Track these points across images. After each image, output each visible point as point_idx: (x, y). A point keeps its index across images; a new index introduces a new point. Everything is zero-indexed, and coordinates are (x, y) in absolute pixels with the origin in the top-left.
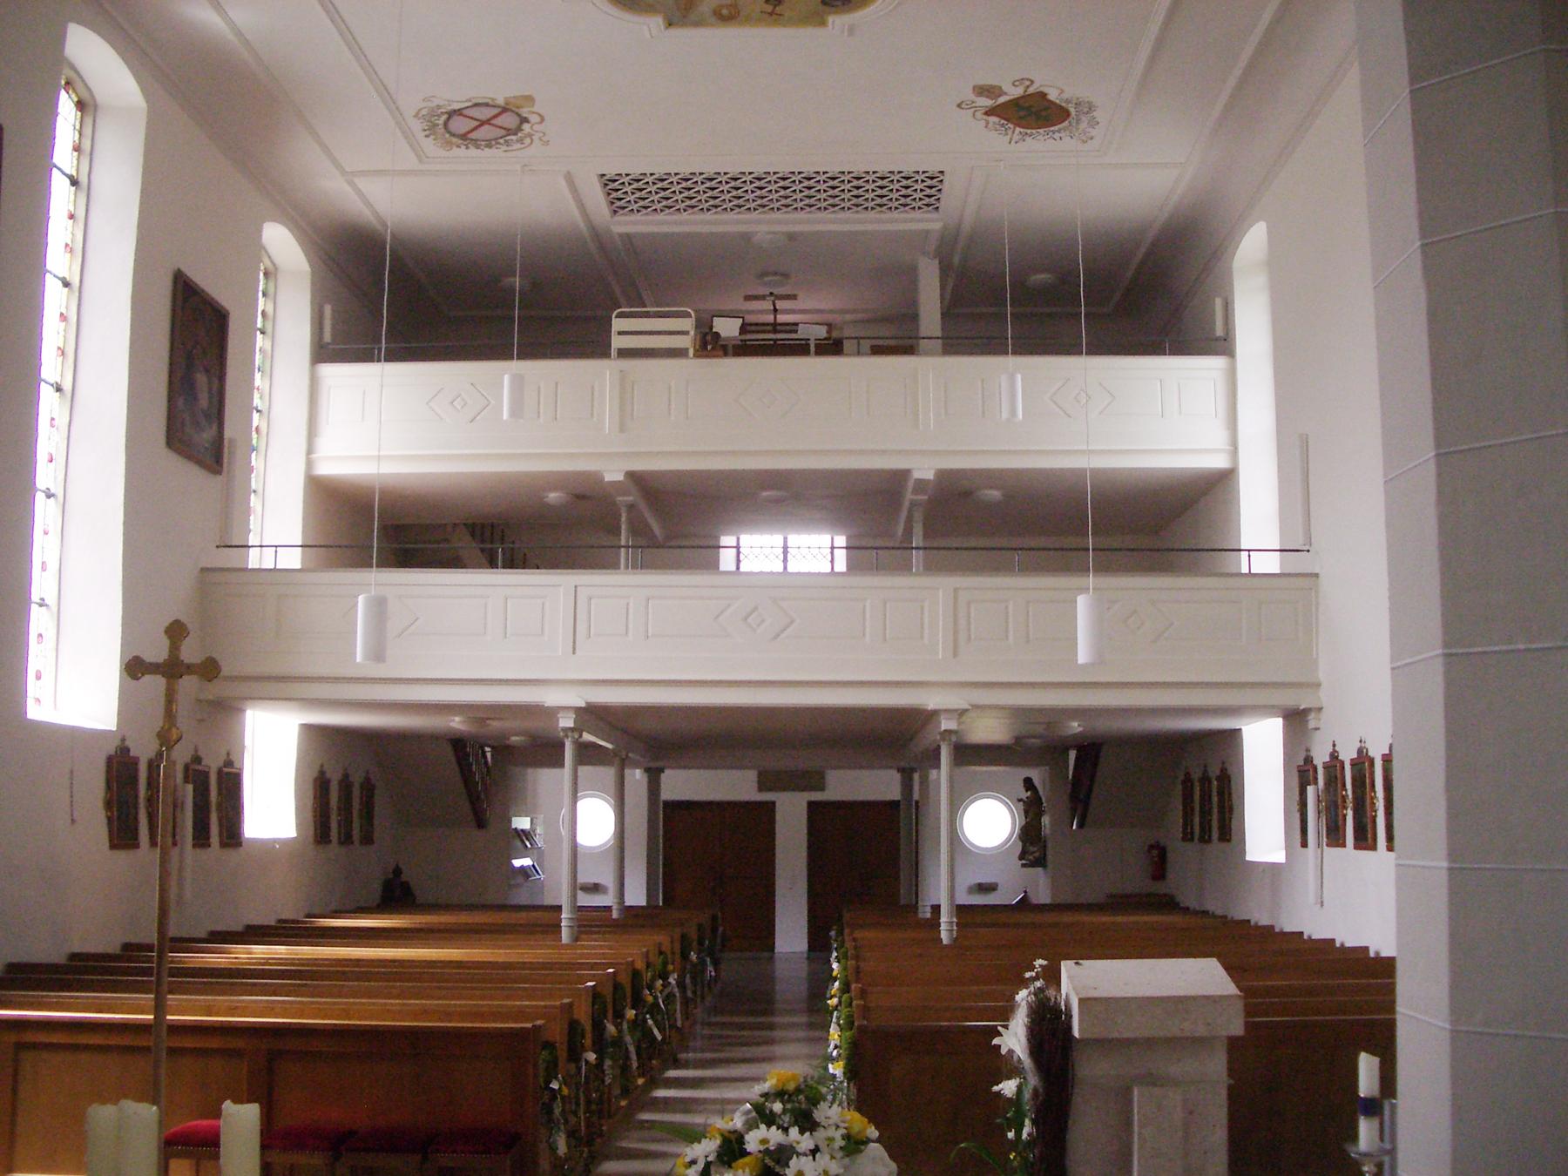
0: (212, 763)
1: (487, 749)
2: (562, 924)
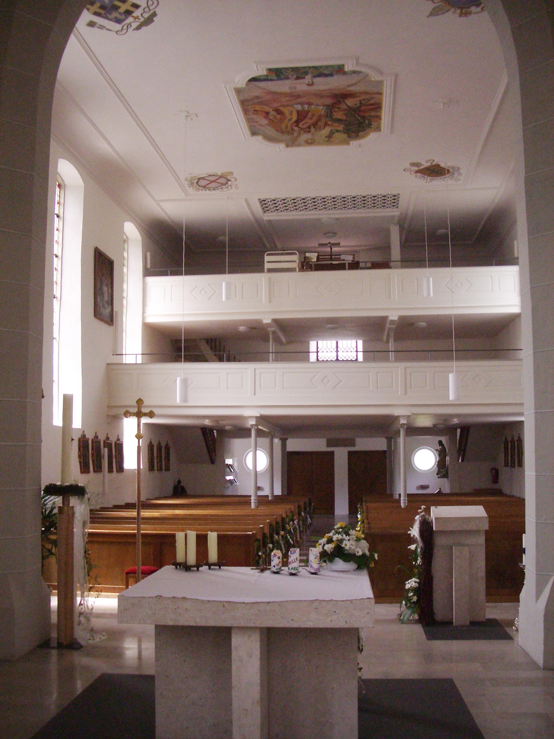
0: (113, 440)
1: (215, 431)
2: (252, 501)
